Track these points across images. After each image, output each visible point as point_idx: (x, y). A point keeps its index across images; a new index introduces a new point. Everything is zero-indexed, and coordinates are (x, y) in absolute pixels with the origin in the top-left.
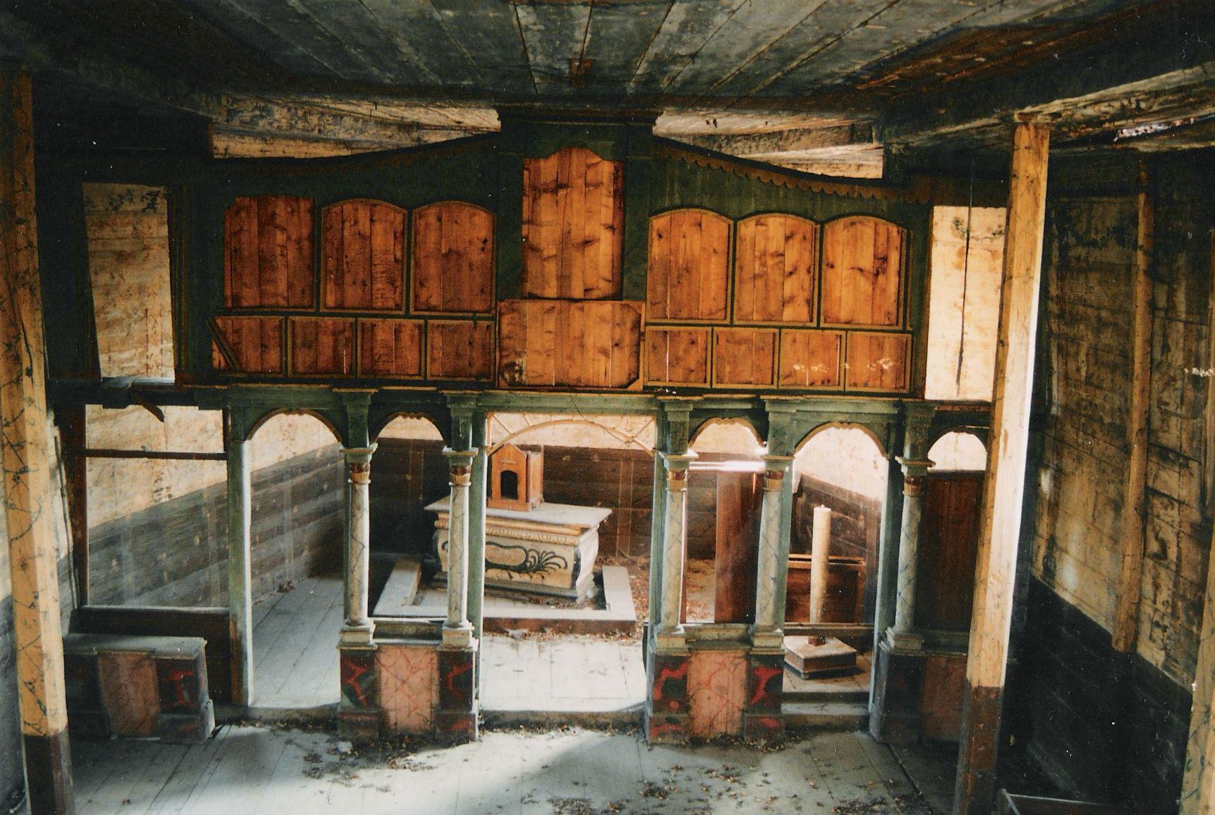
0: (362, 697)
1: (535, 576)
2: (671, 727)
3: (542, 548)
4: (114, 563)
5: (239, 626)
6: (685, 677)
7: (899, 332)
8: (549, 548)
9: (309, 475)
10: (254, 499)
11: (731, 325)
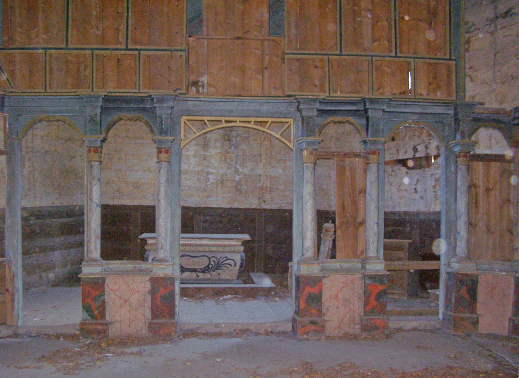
0: (96, 312)
1: (214, 273)
2: (312, 327)
3: (219, 256)
5: (13, 268)
6: (321, 292)
7: (447, 60)
9: (71, 219)
11: (340, 55)
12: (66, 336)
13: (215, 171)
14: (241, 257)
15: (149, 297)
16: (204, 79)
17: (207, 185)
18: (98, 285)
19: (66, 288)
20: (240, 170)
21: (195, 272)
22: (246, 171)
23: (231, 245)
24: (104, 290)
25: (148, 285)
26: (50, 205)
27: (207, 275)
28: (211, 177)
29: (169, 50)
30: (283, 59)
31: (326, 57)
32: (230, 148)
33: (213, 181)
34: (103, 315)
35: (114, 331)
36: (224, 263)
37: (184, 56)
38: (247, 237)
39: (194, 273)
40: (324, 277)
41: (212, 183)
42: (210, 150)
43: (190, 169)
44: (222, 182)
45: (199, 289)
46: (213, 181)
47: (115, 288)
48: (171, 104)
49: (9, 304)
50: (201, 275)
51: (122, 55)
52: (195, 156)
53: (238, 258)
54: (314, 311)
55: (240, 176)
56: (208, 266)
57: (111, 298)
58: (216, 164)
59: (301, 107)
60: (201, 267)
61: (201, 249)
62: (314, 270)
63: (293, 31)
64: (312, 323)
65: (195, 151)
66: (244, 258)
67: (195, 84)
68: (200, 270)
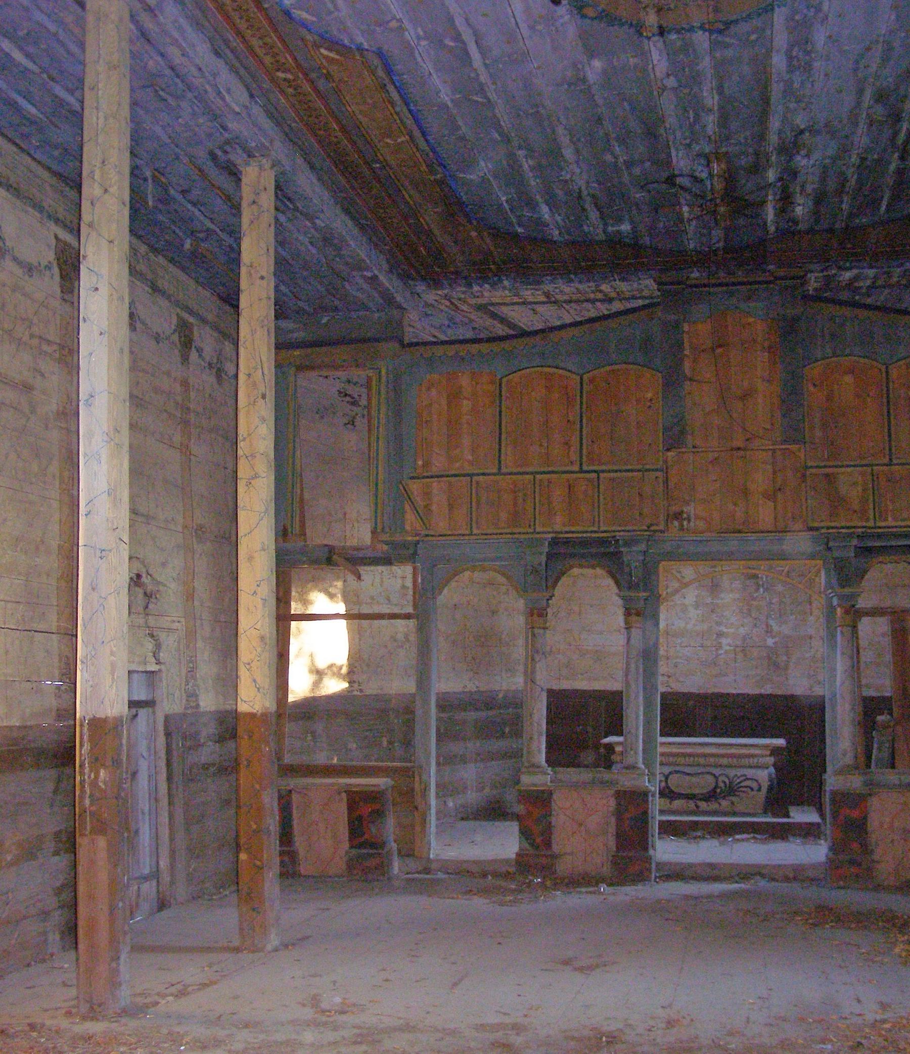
0: (538, 840)
3: (732, 773)
4: (309, 738)
5: (424, 777)
8: (739, 772)
9: (491, 713)
10: (439, 719)
12: (496, 875)
13: (732, 630)
14: (770, 775)
15: (613, 820)
16: (690, 509)
17: (717, 655)
18: (541, 801)
19: (483, 823)
20: (775, 628)
21: (691, 799)
22: (786, 630)
23: (755, 757)
24: (550, 807)
25: (613, 803)
26: (461, 690)
27: (714, 806)
28: (724, 641)
29: (639, 471)
30: (804, 476)
31: (869, 469)
32: (757, 590)
33: (728, 648)
34: (548, 844)
35: (563, 867)
36: (742, 784)
37: (661, 480)
38: (781, 742)
39: (691, 802)
40: (870, 795)
41: (726, 652)
42: (722, 595)
43: (689, 627)
44: (744, 649)
45: (696, 823)
46: (728, 648)
47: (564, 808)
48: (642, 547)
49: (418, 829)
50: (703, 805)
51: (577, 479)
52: (697, 606)
53: (764, 776)
54: (856, 846)
55: (777, 639)
56: (714, 790)
57: (560, 819)
58: (733, 619)
59: (831, 544)
60: (701, 792)
61: (702, 761)
62: (855, 782)
63: (818, 433)
64: (852, 862)
65: (697, 596)
66: (774, 776)
67: (678, 516)
68: (700, 796)
